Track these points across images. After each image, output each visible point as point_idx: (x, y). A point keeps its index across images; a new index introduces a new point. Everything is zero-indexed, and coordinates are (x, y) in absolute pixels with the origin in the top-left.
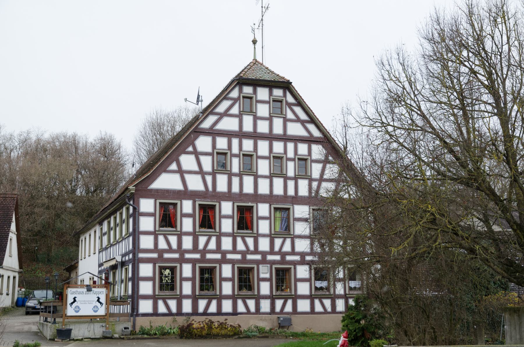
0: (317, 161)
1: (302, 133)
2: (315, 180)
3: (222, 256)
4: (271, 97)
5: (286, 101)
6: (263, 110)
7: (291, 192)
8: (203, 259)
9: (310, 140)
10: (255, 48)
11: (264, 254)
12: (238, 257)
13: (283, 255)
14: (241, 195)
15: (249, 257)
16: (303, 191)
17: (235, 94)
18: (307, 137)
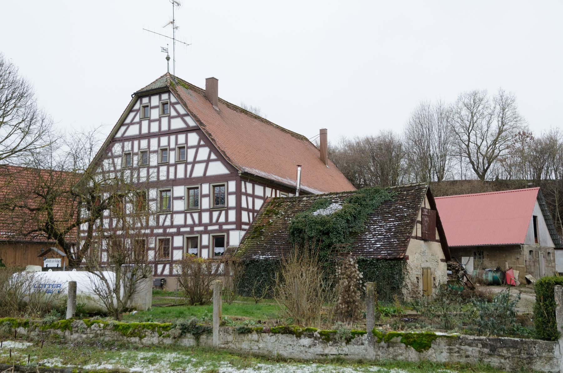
0: (192, 147)
1: (182, 125)
2: (190, 163)
3: (177, 230)
4: (142, 105)
5: (170, 102)
6: (155, 114)
7: (172, 176)
8: (138, 235)
9: (187, 131)
10: (168, 64)
11: (206, 226)
12: (188, 229)
13: (165, 228)
14: (139, 185)
15: (196, 229)
16: (181, 174)
17: (137, 106)
18: (185, 128)
